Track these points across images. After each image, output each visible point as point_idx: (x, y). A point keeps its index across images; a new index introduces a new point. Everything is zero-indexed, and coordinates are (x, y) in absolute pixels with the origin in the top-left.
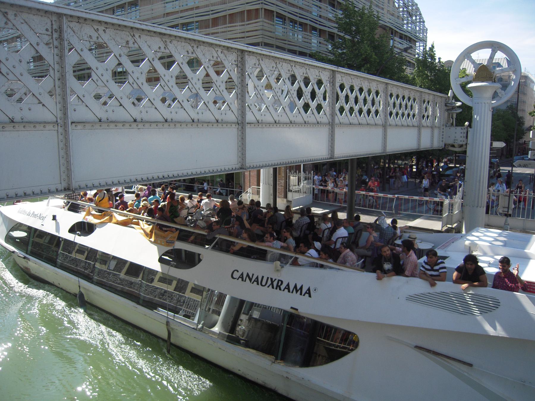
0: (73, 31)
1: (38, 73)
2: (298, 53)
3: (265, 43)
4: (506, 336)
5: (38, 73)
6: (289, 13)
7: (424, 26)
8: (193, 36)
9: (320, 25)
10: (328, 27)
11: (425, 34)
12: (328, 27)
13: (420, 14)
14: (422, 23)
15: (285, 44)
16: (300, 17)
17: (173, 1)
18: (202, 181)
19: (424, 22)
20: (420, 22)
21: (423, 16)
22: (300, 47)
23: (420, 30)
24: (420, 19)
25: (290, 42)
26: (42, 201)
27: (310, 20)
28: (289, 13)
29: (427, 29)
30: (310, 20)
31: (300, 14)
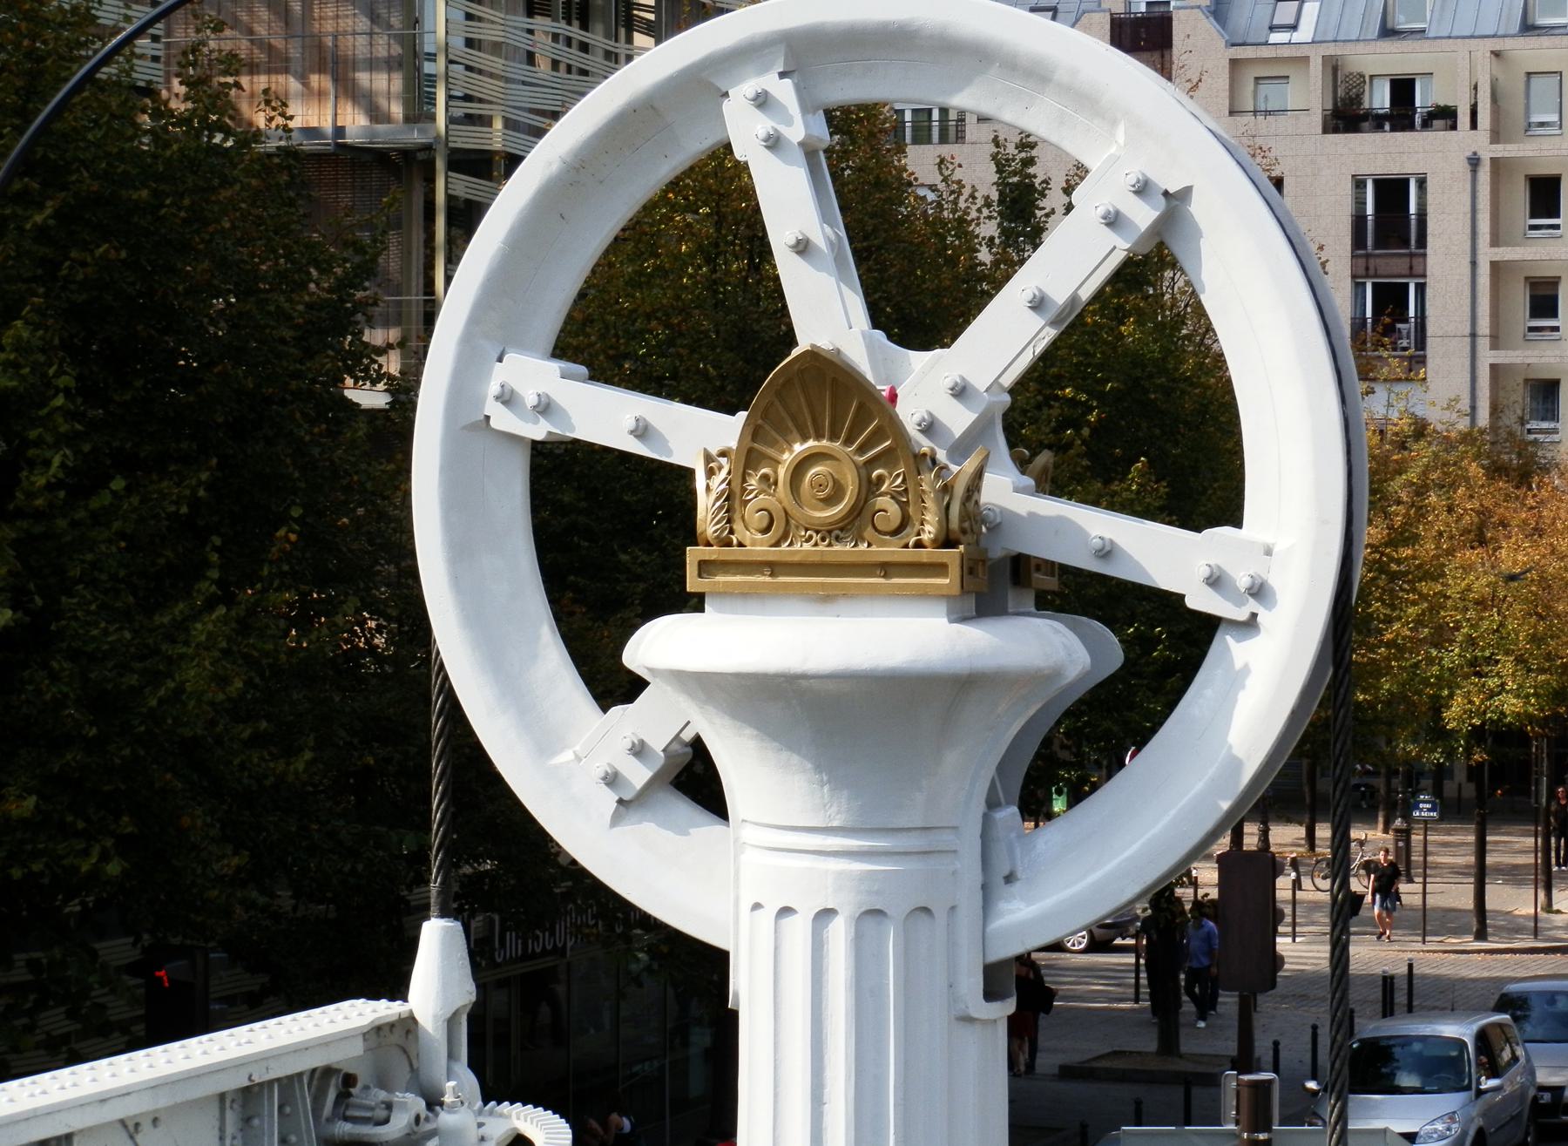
26: (733, 1016)
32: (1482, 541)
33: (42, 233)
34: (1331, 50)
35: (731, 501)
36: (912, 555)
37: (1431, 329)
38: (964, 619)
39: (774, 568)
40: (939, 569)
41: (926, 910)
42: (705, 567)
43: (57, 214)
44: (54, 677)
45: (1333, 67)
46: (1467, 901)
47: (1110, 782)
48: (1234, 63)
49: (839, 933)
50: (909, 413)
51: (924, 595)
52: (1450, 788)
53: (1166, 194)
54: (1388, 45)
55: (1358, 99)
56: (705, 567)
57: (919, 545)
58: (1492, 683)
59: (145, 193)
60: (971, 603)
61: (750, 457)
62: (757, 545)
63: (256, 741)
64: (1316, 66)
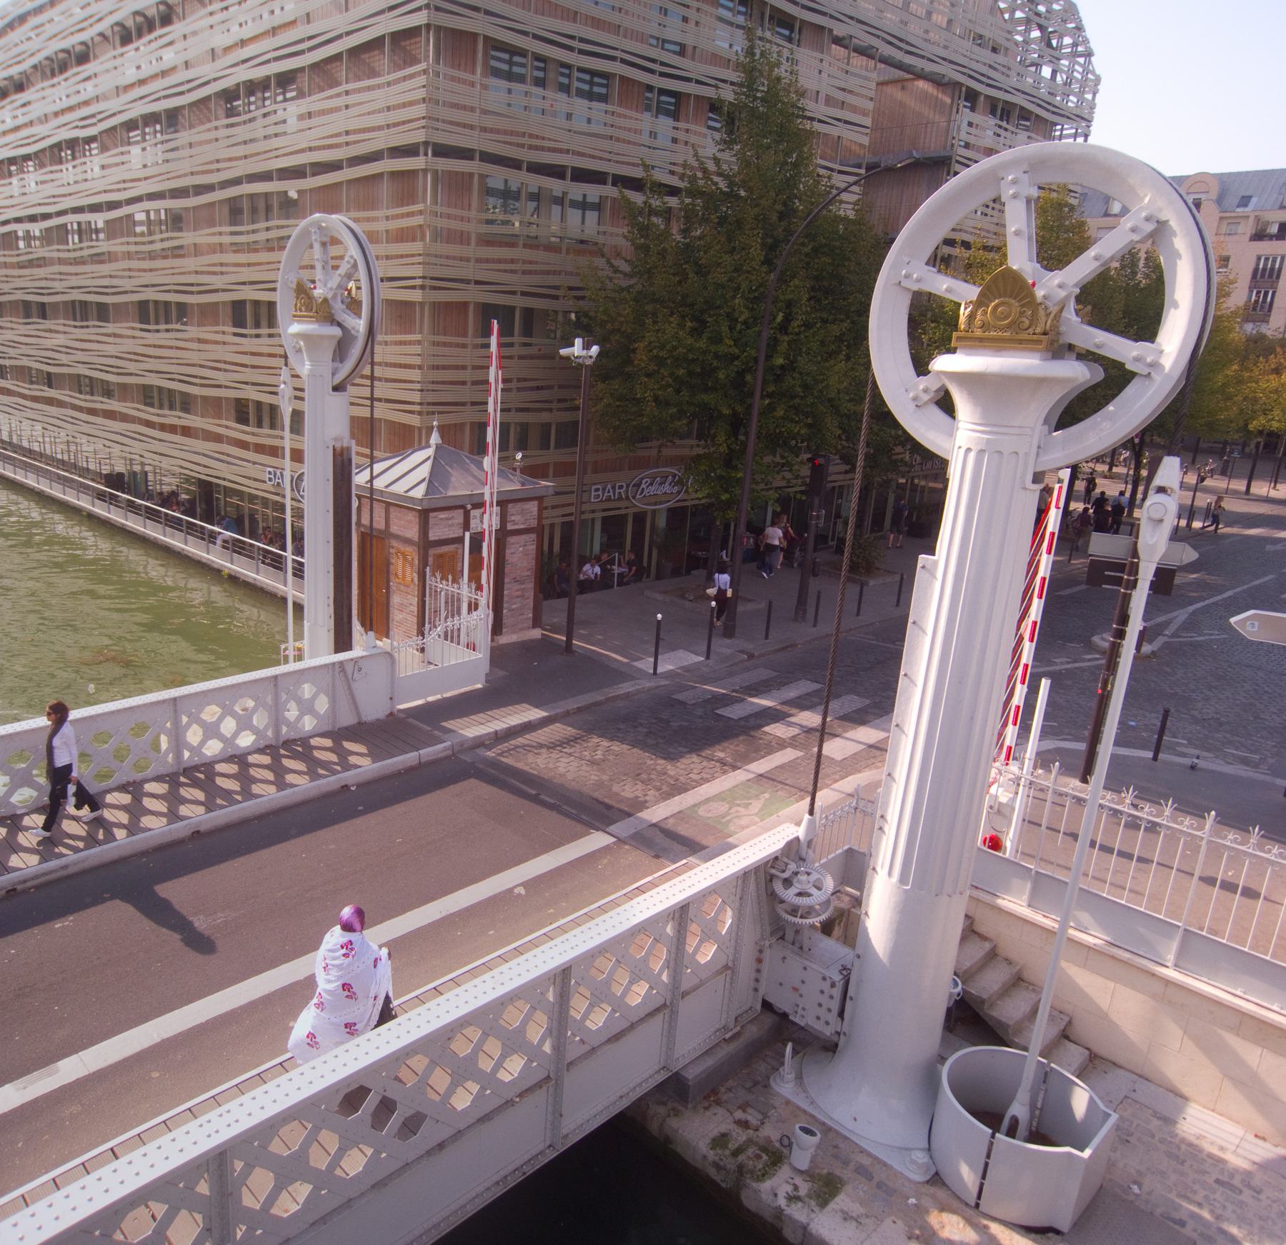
0: (74, 146)
1: (14, 277)
2: (610, 180)
3: (435, 145)
4: (881, 955)
5: (14, 277)
6: (536, 37)
7: (1087, 70)
8: (64, 122)
9: (662, 74)
10: (698, 82)
11: (1089, 96)
12: (698, 82)
13: (1079, 28)
14: (1081, 60)
15: (522, 146)
16: (581, 52)
17: (39, 10)
18: (1103, 456)
19: (1089, 54)
20: (1074, 55)
21: (1091, 32)
22: (575, 153)
23: (1067, 84)
24: (1075, 45)
25: (537, 137)
26: (948, 480)
27: (623, 61)
28: (536, 37)
29: (1098, 80)
30: (623, 61)
31: (582, 40)
32: (1277, 373)
33: (807, 255)
34: (1257, 214)
35: (971, 317)
36: (1030, 337)
37: (1275, 305)
38: (1046, 360)
39: (981, 340)
40: (1039, 342)
41: (1017, 453)
42: (959, 338)
43: (812, 249)
44: (794, 379)
45: (1258, 219)
46: (1244, 488)
47: (906, 317)
48: (1221, 218)
49: (972, 456)
50: (1040, 293)
51: (1033, 350)
52: (1247, 450)
53: (1158, 222)
54: (1281, 212)
55: (1265, 230)
56: (959, 338)
57: (1034, 334)
58: (1270, 417)
59: (838, 243)
60: (1050, 355)
61: (980, 303)
62: (978, 333)
63: (850, 400)
64: (1252, 219)
